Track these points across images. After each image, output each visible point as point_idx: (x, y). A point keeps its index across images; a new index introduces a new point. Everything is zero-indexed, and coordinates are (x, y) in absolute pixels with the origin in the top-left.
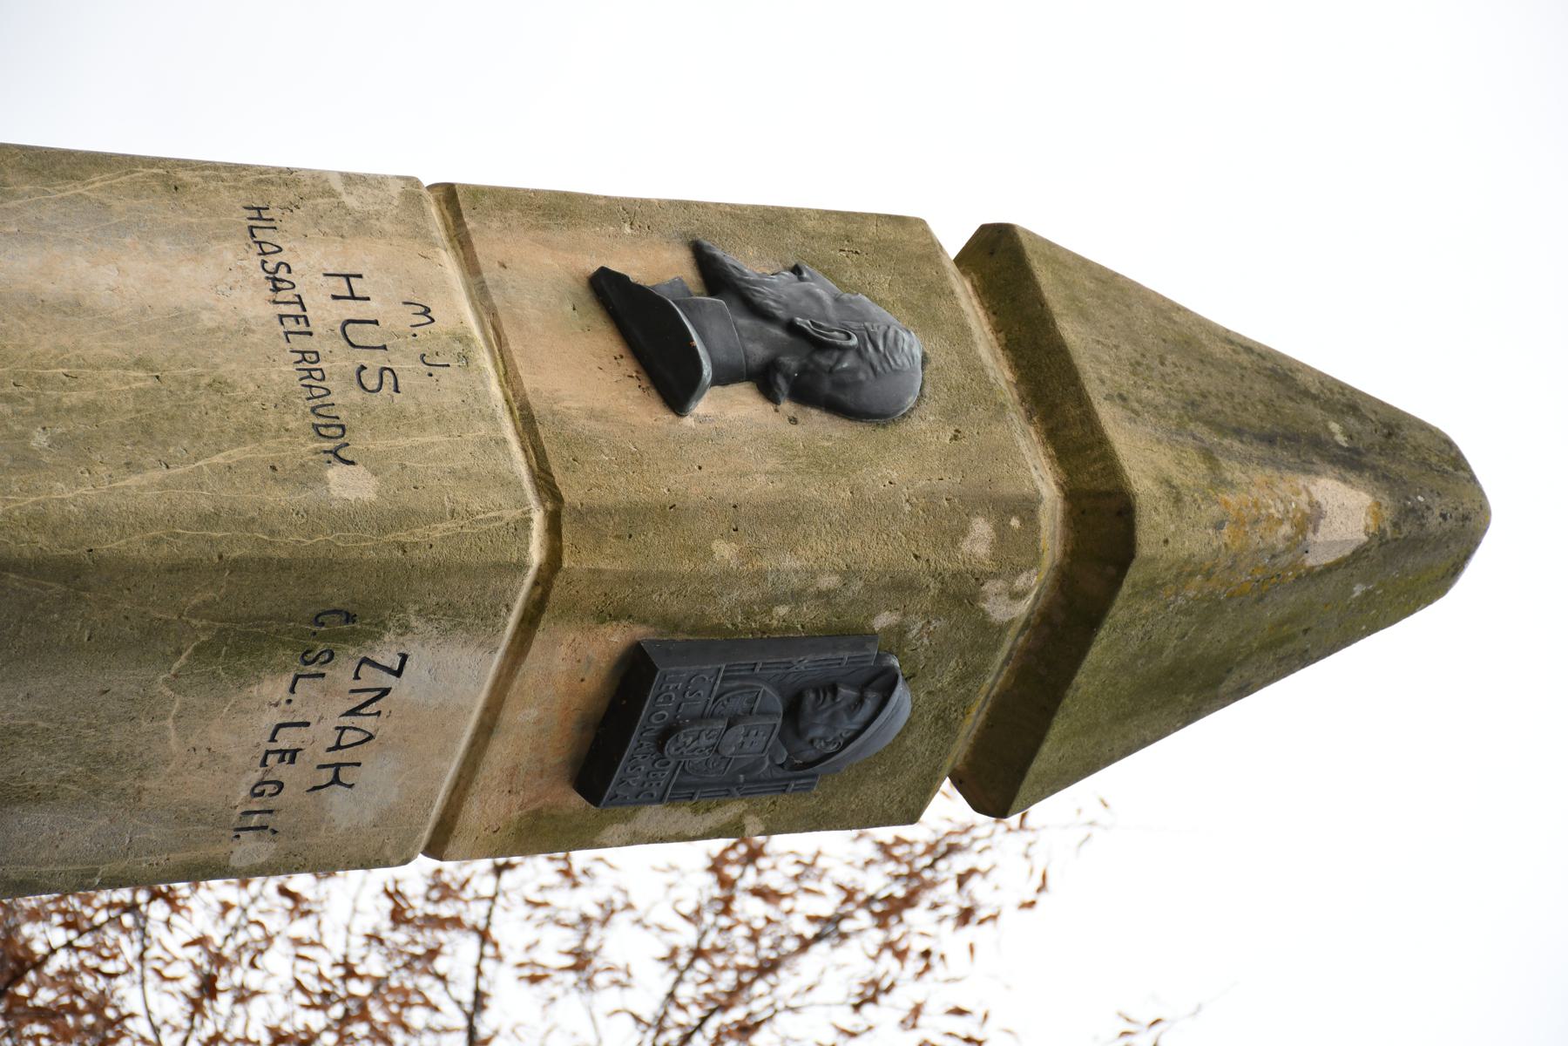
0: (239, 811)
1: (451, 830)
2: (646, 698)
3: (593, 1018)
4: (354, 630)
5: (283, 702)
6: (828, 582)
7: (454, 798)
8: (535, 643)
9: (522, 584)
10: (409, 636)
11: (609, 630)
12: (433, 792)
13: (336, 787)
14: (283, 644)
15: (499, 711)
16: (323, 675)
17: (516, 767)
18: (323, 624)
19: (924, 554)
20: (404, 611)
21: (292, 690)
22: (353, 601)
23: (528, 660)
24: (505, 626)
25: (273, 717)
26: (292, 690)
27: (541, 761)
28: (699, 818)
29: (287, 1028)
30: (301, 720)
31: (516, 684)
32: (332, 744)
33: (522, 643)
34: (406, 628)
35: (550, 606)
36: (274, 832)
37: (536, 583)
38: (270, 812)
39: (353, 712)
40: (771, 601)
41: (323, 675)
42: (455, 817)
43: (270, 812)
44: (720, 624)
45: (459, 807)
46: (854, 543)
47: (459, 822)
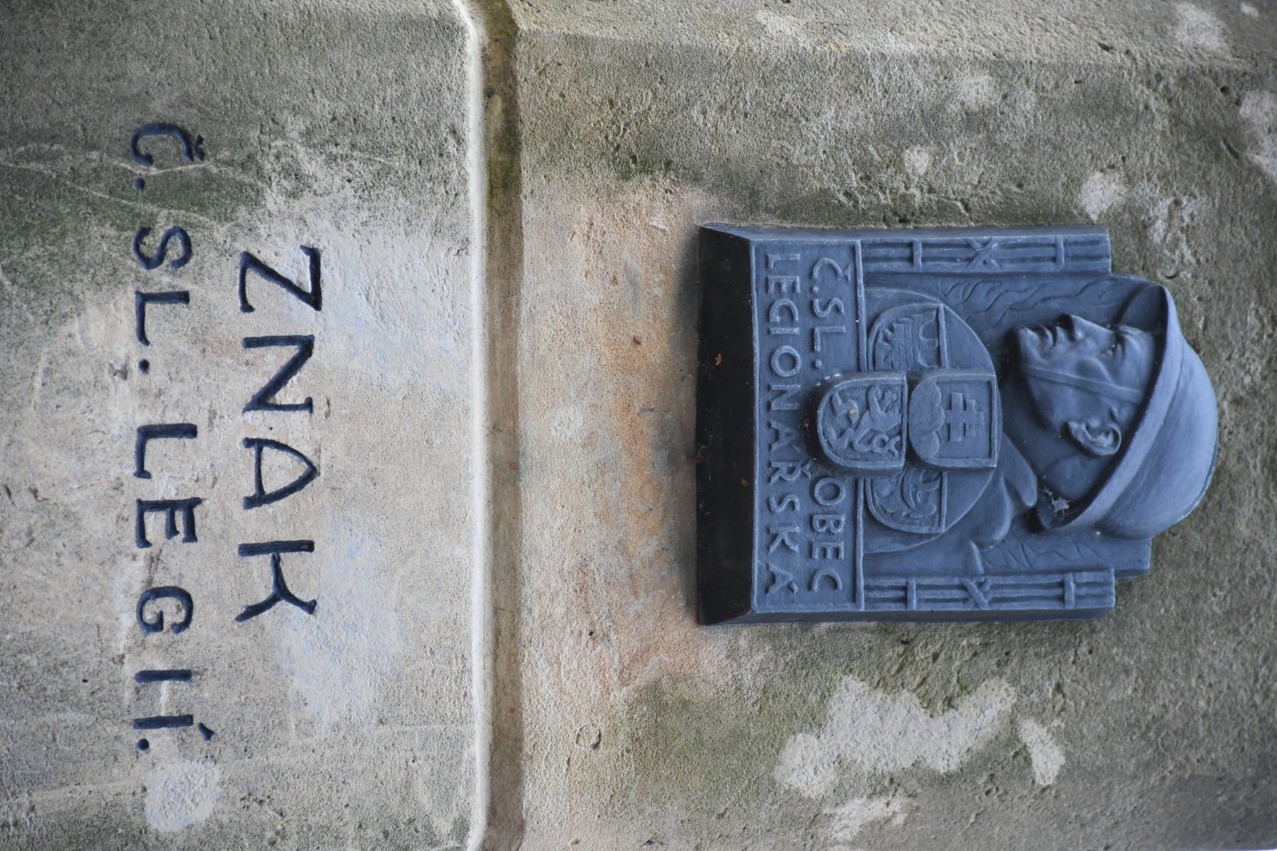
0: (130, 670)
1: (518, 741)
2: (749, 313)
3: (990, 440)
4: (209, 181)
5: (134, 366)
6: (975, 89)
7: (502, 670)
8: (527, 230)
9: (463, 74)
10: (307, 199)
11: (641, 197)
12: (456, 624)
13: (283, 605)
14: (94, 206)
15: (514, 416)
16: (184, 297)
17: (583, 567)
18: (149, 159)
19: (1121, 43)
20: (282, 133)
21: (142, 336)
22: (187, 100)
23: (528, 275)
24: (464, 181)
25: (125, 411)
26: (142, 336)
27: (622, 547)
28: (939, 723)
29: (144, 499)
30: (173, 418)
31: (524, 341)
32: (251, 491)
33: (506, 240)
34: (299, 183)
35: (525, 130)
36: (208, 733)
37: (488, 93)
38: (185, 675)
39: (262, 401)
40: (897, 136)
41: (184, 297)
42: (515, 710)
43: (185, 675)
44: (824, 192)
45: (515, 683)
46: (990, 27)
47: (527, 717)
